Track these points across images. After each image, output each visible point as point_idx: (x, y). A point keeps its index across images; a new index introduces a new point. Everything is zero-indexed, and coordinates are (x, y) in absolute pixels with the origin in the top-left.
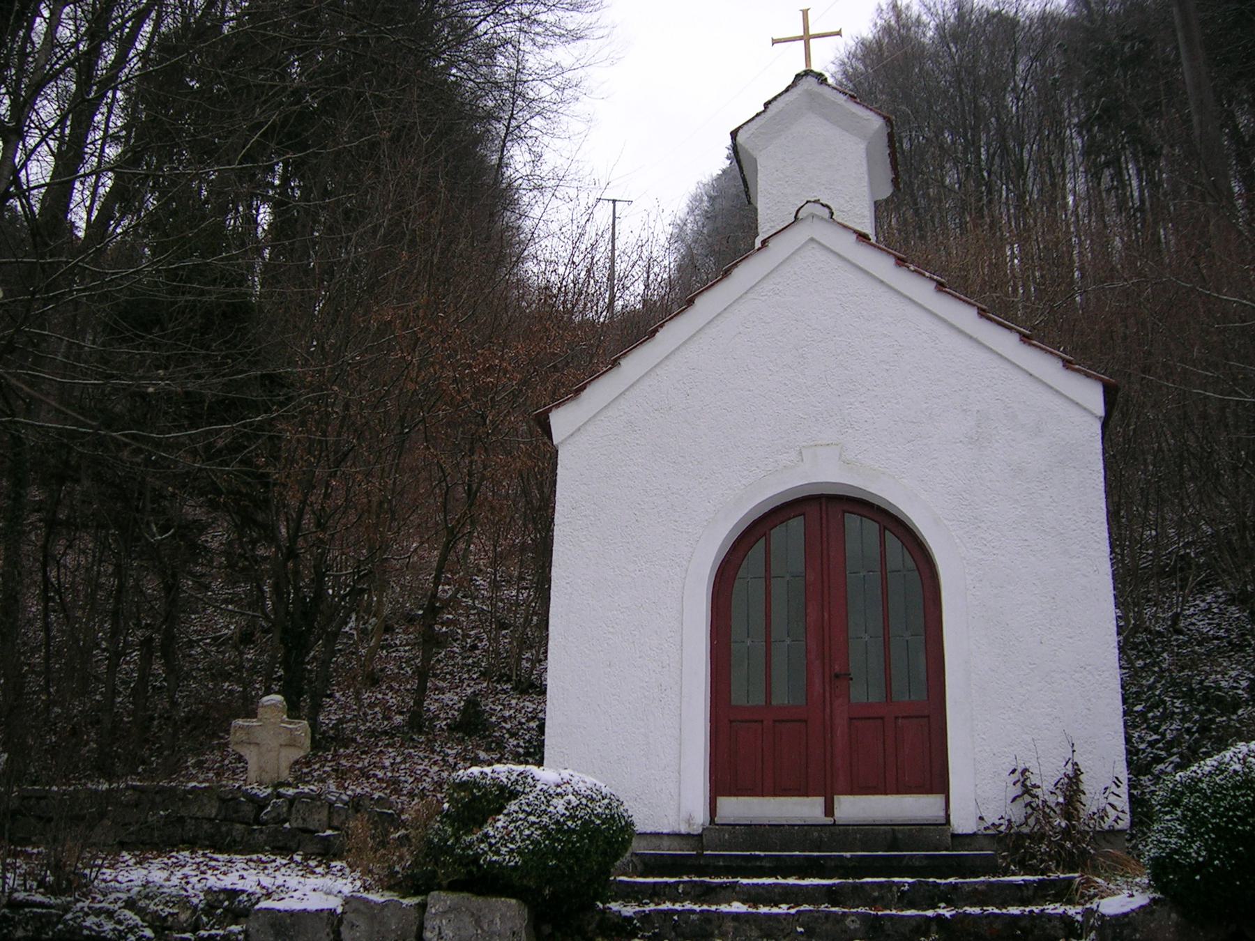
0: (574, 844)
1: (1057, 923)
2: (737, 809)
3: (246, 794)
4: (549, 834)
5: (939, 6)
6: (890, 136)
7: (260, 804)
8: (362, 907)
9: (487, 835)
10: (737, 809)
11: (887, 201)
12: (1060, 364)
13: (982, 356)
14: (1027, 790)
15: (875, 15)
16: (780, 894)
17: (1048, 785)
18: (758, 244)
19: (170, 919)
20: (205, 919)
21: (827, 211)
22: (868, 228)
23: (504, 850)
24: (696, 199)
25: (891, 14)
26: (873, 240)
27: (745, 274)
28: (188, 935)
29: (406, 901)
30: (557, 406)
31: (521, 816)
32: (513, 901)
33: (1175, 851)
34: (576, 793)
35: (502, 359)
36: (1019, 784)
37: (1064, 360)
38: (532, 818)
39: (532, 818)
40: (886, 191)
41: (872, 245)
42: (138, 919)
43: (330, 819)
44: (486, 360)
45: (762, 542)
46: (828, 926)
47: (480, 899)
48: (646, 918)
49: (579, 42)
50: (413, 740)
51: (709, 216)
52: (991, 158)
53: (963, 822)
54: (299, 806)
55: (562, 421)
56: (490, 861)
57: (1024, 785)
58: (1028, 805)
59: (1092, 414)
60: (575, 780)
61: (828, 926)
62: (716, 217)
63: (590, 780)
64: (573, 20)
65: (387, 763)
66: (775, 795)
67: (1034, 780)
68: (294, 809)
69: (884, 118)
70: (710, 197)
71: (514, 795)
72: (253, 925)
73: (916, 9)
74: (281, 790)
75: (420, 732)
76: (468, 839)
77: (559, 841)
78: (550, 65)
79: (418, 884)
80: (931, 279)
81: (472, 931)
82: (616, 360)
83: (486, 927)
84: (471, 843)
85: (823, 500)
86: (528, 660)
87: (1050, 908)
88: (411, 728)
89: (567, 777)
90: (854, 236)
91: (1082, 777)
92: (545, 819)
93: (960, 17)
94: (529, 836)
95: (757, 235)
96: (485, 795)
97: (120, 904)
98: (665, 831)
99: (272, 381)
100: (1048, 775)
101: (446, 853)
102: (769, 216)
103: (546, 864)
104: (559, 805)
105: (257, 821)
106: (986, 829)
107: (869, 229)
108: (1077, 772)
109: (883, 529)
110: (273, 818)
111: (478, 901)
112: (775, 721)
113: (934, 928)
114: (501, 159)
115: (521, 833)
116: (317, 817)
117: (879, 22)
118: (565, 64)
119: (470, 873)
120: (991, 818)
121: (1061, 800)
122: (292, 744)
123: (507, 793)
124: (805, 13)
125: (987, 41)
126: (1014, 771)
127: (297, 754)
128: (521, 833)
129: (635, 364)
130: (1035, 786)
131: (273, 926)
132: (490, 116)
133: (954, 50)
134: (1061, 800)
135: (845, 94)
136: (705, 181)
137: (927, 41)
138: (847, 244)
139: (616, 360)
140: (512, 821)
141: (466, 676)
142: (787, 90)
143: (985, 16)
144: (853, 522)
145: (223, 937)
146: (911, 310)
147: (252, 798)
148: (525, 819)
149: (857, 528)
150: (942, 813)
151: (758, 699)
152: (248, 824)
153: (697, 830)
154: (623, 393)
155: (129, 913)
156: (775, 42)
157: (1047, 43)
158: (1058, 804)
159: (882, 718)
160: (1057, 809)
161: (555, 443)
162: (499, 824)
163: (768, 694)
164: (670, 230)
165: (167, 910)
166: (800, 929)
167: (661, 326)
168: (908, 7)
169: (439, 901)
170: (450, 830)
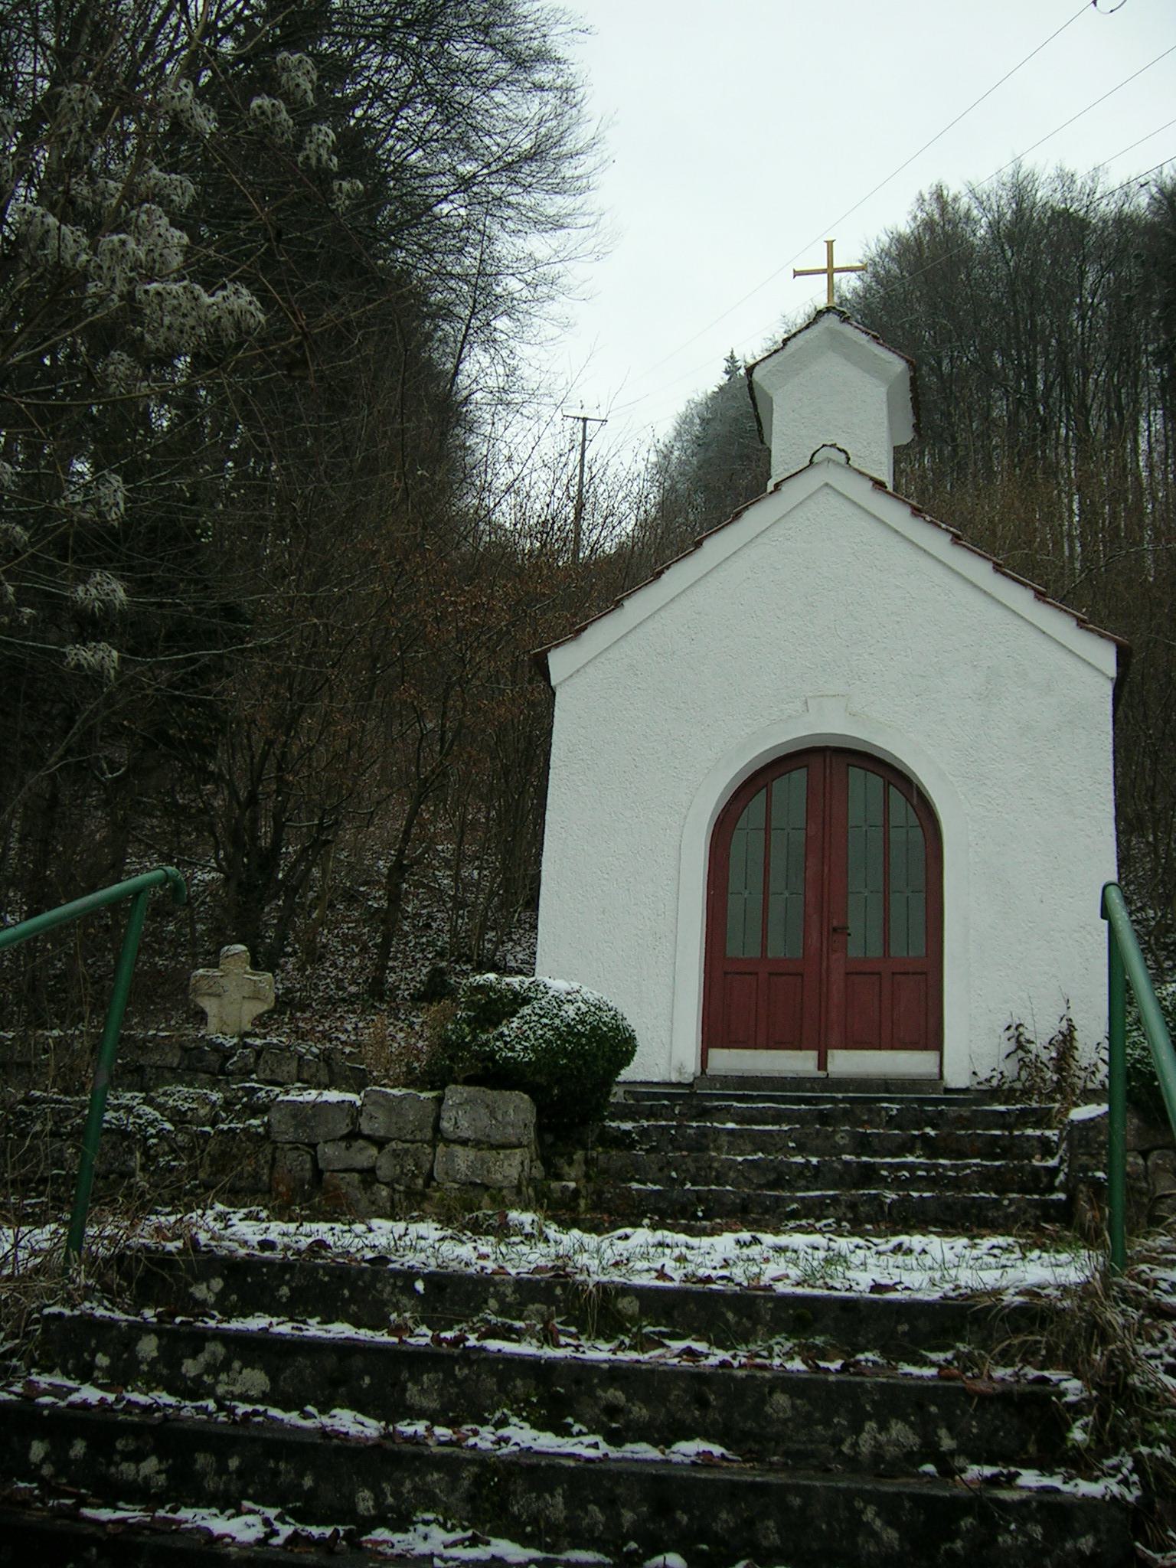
0: (583, 1046)
1: (1035, 1143)
2: (728, 1061)
3: (210, 1043)
4: (560, 1035)
5: (993, 199)
6: (913, 381)
7: (226, 1054)
8: (381, 1100)
9: (502, 1035)
10: (728, 1061)
11: (908, 446)
12: (1074, 623)
13: (997, 613)
14: (1020, 1046)
15: (916, 206)
16: (773, 1117)
17: (1042, 1040)
18: (770, 487)
19: (189, 1113)
20: (224, 1115)
21: (843, 456)
22: (886, 476)
23: (518, 1047)
24: (685, 421)
25: (935, 205)
26: (890, 488)
27: (756, 517)
28: (207, 1129)
29: (423, 1095)
30: (557, 646)
31: (536, 1018)
32: (526, 1096)
33: (1138, 1061)
34: (585, 1001)
35: (492, 597)
36: (1013, 1040)
37: (1078, 619)
38: (544, 1020)
39: (544, 1020)
40: (907, 436)
41: (888, 493)
42: (157, 1114)
43: (299, 1072)
44: (474, 597)
45: (761, 797)
46: (818, 1142)
47: (495, 1093)
48: (644, 1132)
49: (559, 232)
50: (375, 1007)
51: (701, 443)
52: (1049, 387)
53: (957, 1076)
54: (268, 1057)
55: (561, 662)
56: (506, 1058)
57: (1018, 1041)
58: (1021, 1059)
59: (1103, 674)
60: (584, 989)
61: (818, 1142)
62: (709, 445)
63: (597, 995)
64: (554, 205)
65: (349, 1028)
66: (768, 1047)
67: (1028, 1035)
68: (261, 1061)
69: (907, 361)
70: (703, 420)
71: (527, 1001)
72: (274, 1116)
73: (964, 202)
74: (249, 1040)
75: (381, 1000)
76: (484, 1037)
77: (570, 1042)
78: (522, 255)
79: (436, 1078)
80: (947, 530)
81: (486, 1121)
82: (619, 601)
83: (500, 1118)
84: (488, 1041)
85: (828, 753)
86: (490, 941)
87: (1029, 1132)
88: (372, 996)
89: (577, 988)
90: (871, 483)
91: (1076, 1034)
92: (557, 1021)
93: (1019, 213)
94: (542, 1036)
95: (769, 477)
96: (500, 998)
97: (137, 1101)
98: (655, 1080)
99: (231, 612)
100: (1042, 1031)
101: (463, 1049)
102: (784, 455)
103: (557, 1063)
104: (570, 1010)
105: (222, 1071)
106: (979, 1083)
107: (886, 477)
108: (1071, 1028)
109: (887, 785)
110: (240, 1069)
111: (492, 1095)
112: (770, 974)
113: (919, 1144)
114: (457, 367)
115: (534, 1033)
116: (286, 1069)
117: (921, 215)
118: (538, 255)
119: (486, 1068)
120: (984, 1074)
121: (1054, 1055)
122: (255, 997)
123: (521, 999)
124: (830, 244)
125: (1050, 244)
126: (1009, 1028)
127: (261, 1008)
128: (534, 1033)
129: (638, 606)
130: (1029, 1042)
131: (294, 1116)
132: (446, 312)
133: (1009, 254)
134: (1054, 1055)
135: (868, 334)
136: (697, 399)
137: (977, 242)
138: (863, 491)
139: (619, 601)
140: (526, 1023)
141: (419, 955)
142: (807, 327)
143: (1049, 214)
144: (856, 775)
145: (242, 1130)
146: (924, 562)
147: (217, 1048)
148: (538, 1021)
149: (862, 785)
150: (936, 1070)
151: (755, 952)
152: (212, 1074)
153: (688, 1078)
154: (626, 635)
155: (148, 1109)
156: (796, 274)
157: (1121, 251)
158: (1052, 1059)
159: (879, 974)
160: (1050, 1064)
161: (553, 683)
162: (514, 1025)
163: (764, 947)
164: (653, 458)
165: (187, 1105)
166: (792, 1145)
167: (668, 568)
168: (955, 199)
169: (455, 1094)
170: (467, 1030)
